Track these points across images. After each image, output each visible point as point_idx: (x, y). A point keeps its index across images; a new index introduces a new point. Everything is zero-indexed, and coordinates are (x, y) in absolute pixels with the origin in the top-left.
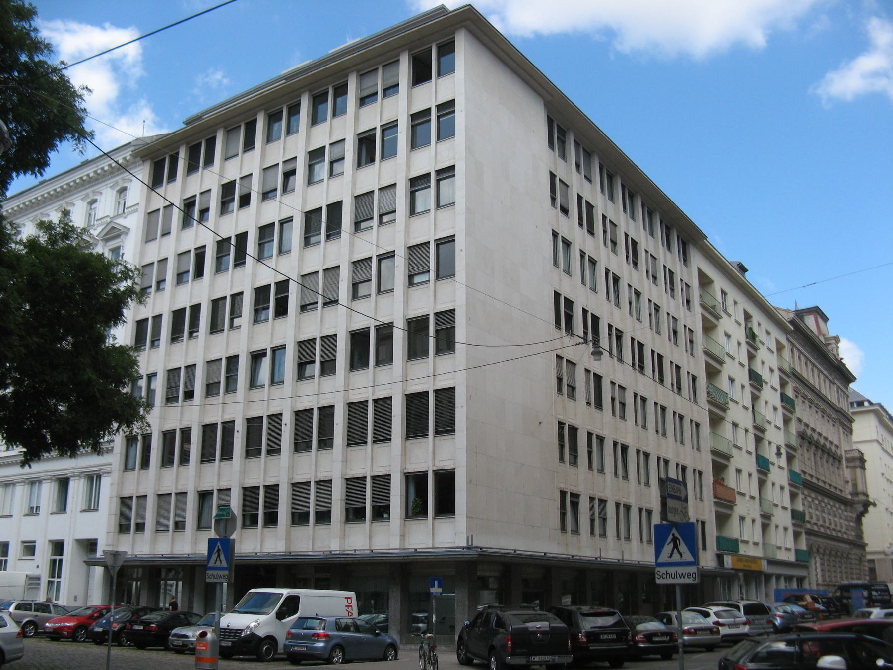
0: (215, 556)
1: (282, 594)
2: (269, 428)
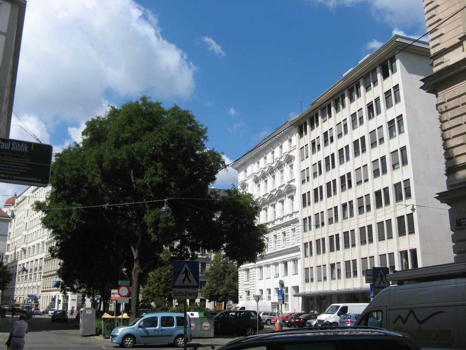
1: (340, 306)
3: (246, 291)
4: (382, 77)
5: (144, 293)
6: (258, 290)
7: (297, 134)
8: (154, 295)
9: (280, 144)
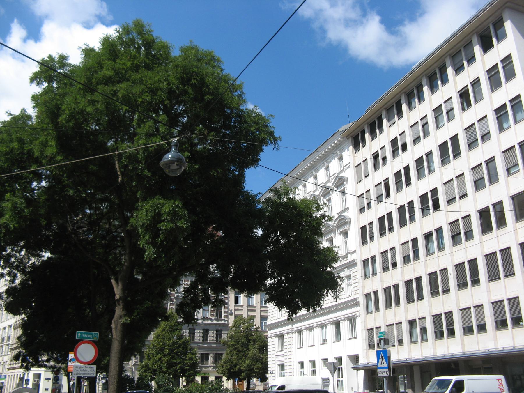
0: (380, 361)
1: (452, 380)
2: (442, 277)
3: (279, 365)
4: (482, 50)
5: (142, 369)
6: (297, 363)
7: (351, 148)
8: (154, 372)
9: (326, 164)
